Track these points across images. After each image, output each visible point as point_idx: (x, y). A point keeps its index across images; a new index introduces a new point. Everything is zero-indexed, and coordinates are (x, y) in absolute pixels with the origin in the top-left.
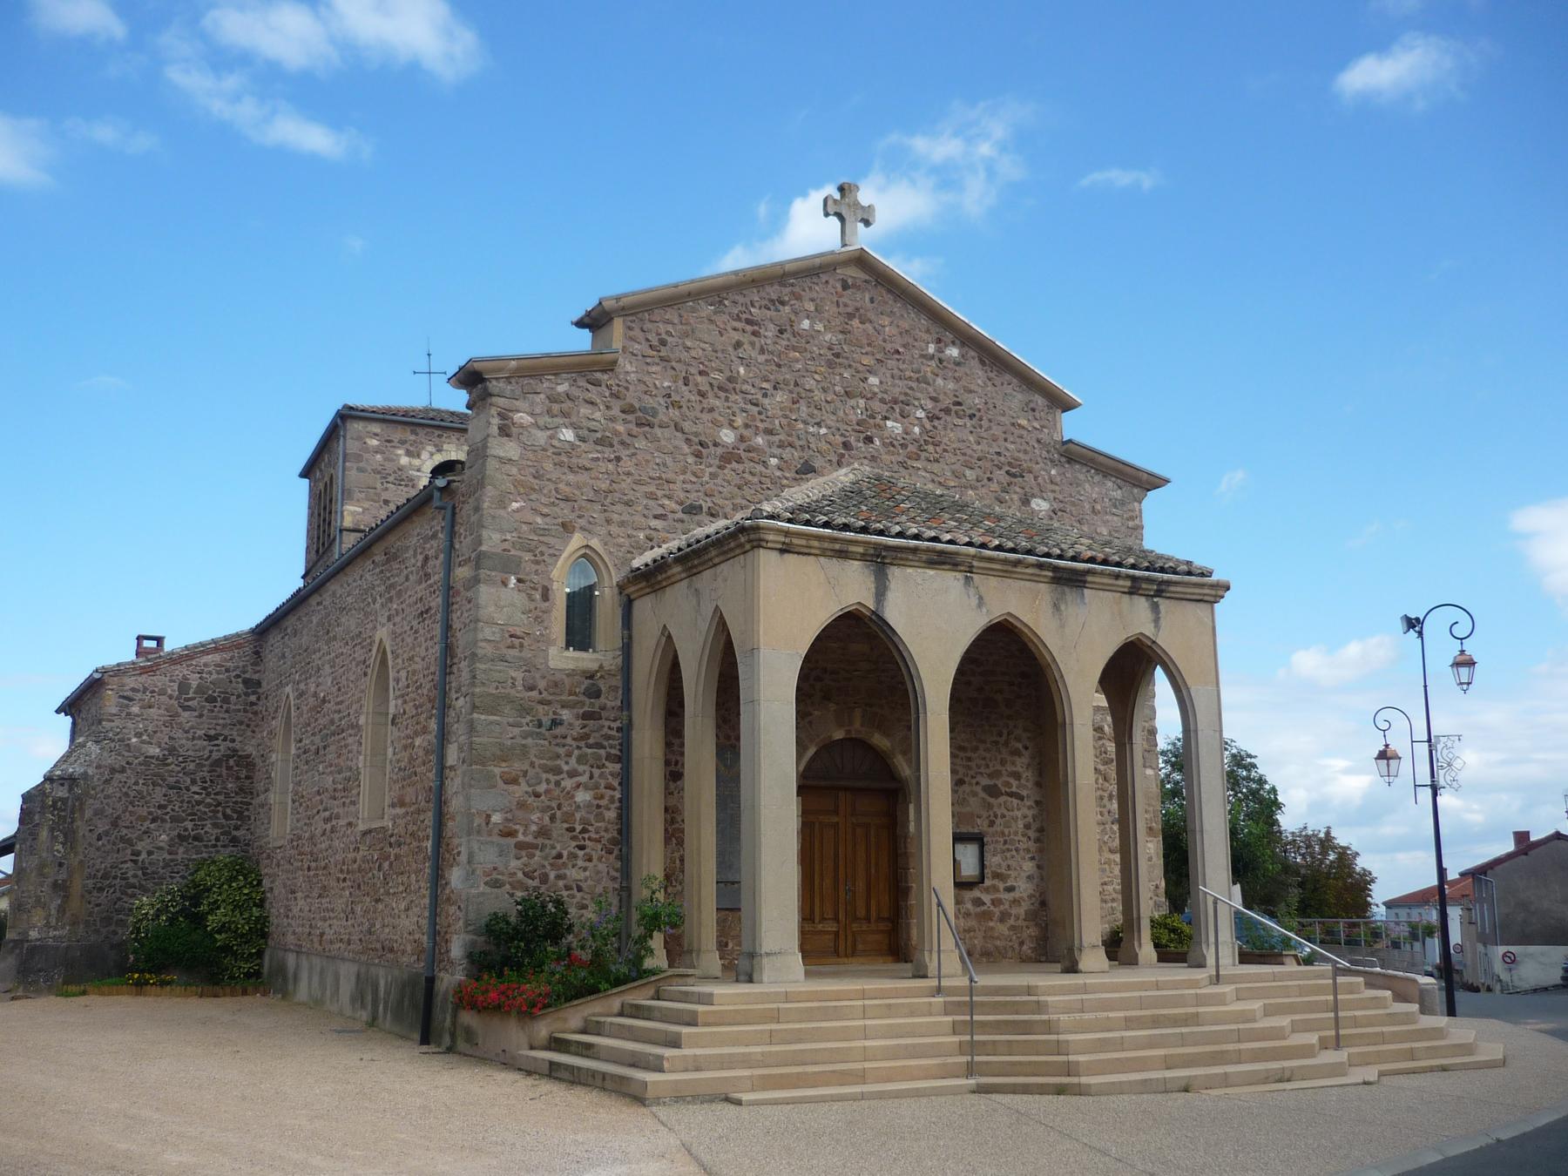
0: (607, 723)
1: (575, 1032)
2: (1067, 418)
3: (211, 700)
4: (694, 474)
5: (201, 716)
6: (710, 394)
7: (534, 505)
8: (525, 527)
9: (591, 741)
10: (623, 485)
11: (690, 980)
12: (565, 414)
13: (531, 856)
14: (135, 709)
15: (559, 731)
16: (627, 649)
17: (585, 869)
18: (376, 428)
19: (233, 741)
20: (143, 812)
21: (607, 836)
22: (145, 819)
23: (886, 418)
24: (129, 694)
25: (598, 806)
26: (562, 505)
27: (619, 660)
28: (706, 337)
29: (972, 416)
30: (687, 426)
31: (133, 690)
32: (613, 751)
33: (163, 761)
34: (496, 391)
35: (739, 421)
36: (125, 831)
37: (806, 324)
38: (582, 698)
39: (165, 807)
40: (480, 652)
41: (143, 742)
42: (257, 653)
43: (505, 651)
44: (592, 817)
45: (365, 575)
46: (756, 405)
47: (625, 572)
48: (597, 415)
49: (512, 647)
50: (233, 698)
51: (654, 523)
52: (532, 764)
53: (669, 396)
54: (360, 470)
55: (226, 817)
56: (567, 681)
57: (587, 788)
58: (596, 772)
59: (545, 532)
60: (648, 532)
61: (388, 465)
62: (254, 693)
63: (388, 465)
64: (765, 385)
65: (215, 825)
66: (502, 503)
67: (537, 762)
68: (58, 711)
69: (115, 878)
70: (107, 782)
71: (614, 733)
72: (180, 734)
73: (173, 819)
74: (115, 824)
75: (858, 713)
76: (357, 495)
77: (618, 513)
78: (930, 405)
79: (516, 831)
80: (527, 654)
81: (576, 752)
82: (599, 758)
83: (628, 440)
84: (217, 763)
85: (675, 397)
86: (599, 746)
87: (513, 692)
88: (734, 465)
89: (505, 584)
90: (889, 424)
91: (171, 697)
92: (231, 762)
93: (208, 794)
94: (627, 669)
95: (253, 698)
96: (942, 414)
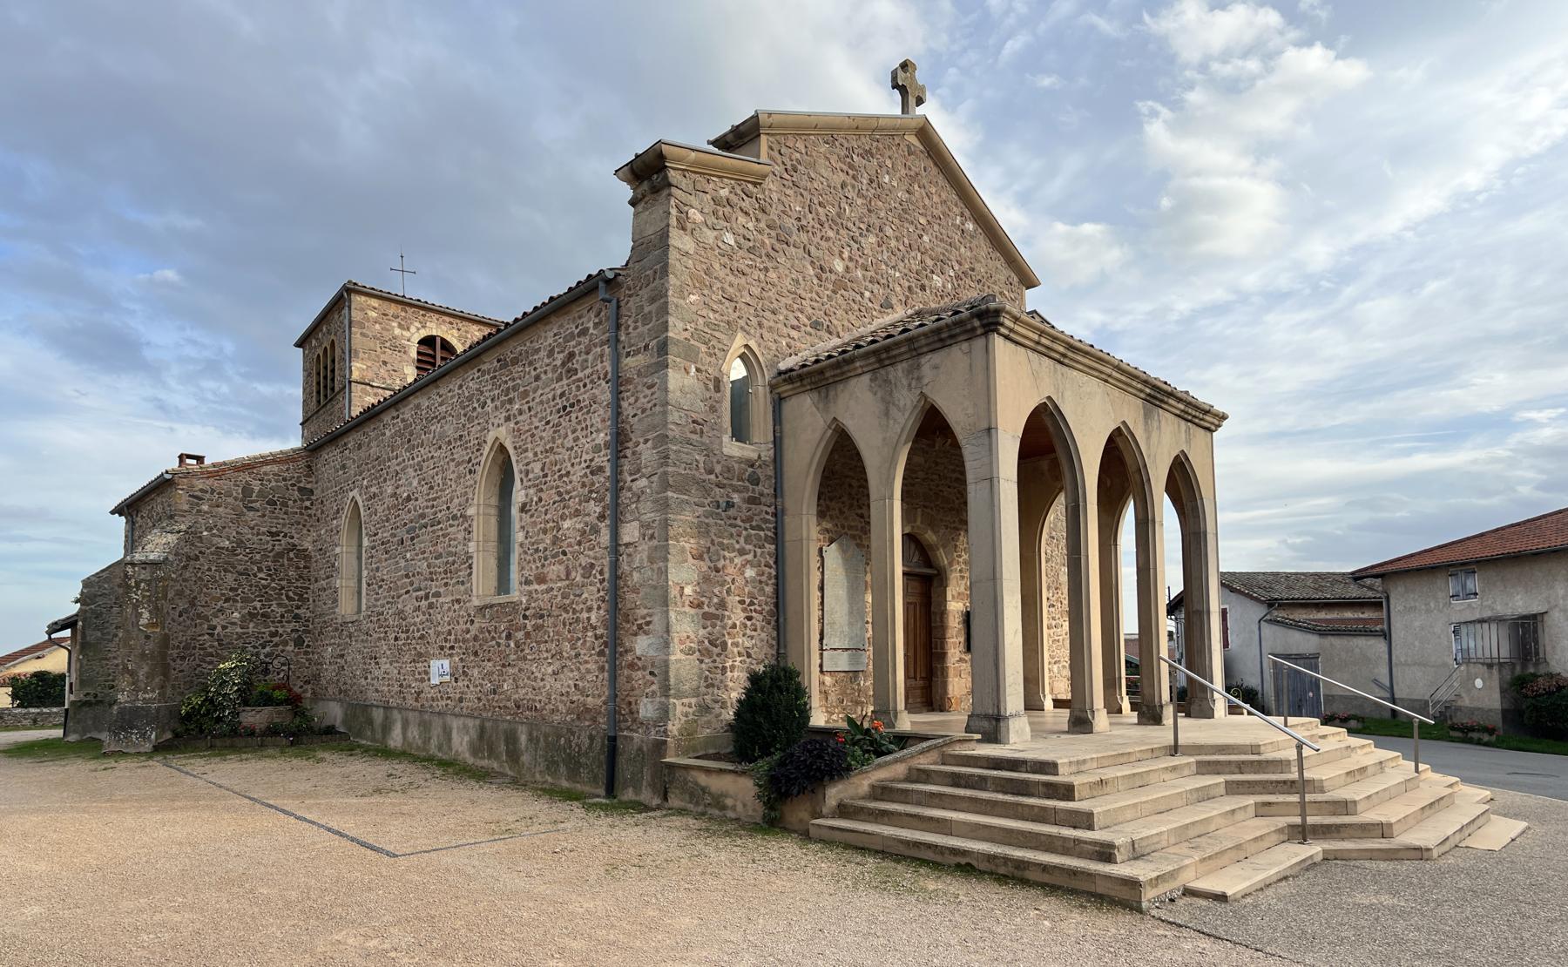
2: (1029, 293)
3: (272, 503)
7: (707, 300)
8: (701, 321)
11: (966, 745)
13: (714, 626)
14: (205, 508)
15: (732, 512)
16: (778, 443)
18: (374, 302)
26: (727, 303)
28: (823, 171)
30: (813, 249)
34: (673, 181)
35: (846, 255)
40: (670, 433)
45: (471, 381)
47: (775, 371)
48: (750, 225)
52: (713, 542)
59: (716, 327)
65: (279, 605)
70: (185, 567)
72: (246, 530)
74: (192, 604)
80: (705, 440)
83: (772, 253)
84: (280, 555)
95: (308, 503)
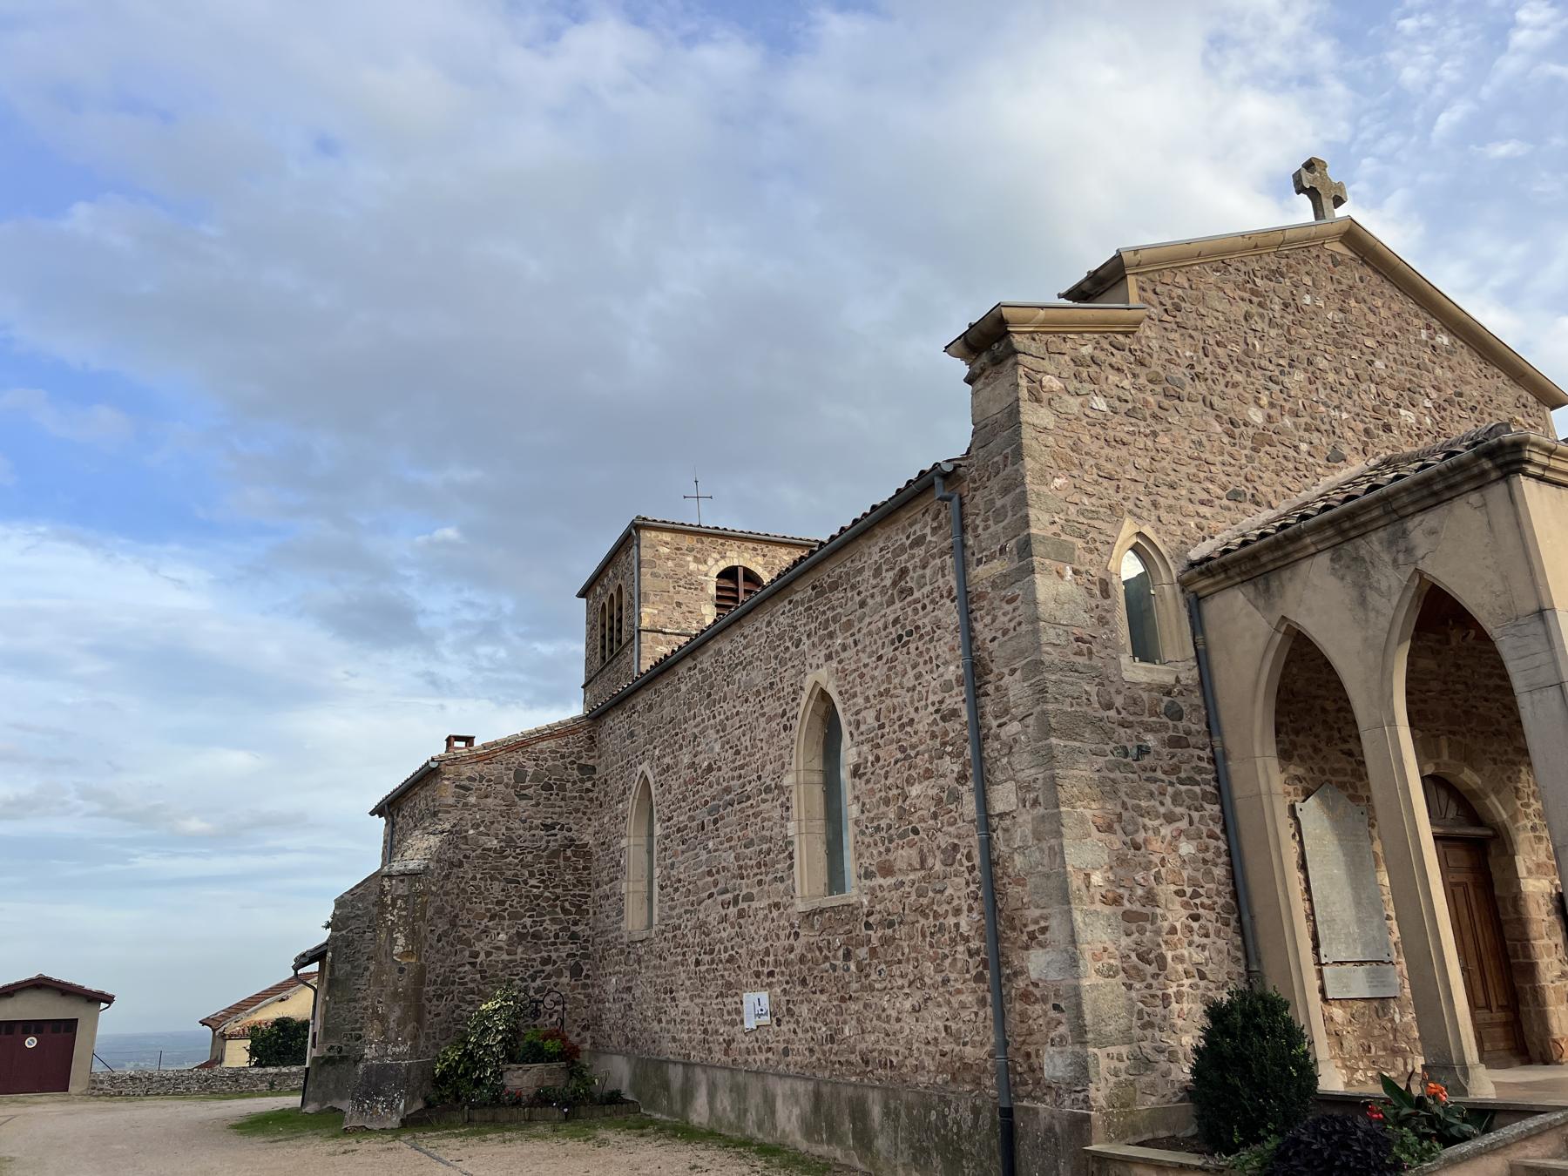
0: (1197, 752)
2: (1557, 416)
4: (1231, 455)
5: (538, 804)
6: (1231, 368)
7: (1078, 482)
8: (1073, 509)
10: (1164, 463)
13: (1142, 931)
14: (472, 800)
15: (1147, 761)
18: (666, 537)
19: (570, 830)
21: (1220, 901)
22: (484, 916)
24: (466, 783)
25: (1205, 861)
26: (1106, 483)
27: (1195, 672)
29: (1473, 409)
30: (1216, 400)
32: (1209, 789)
33: (501, 853)
34: (1020, 347)
35: (1264, 401)
36: (463, 931)
37: (1308, 299)
38: (1165, 719)
39: (503, 903)
40: (1046, 658)
41: (481, 834)
42: (591, 738)
44: (1199, 875)
45: (781, 616)
48: (1126, 383)
49: (1079, 653)
50: (569, 785)
51: (1204, 510)
53: (1192, 367)
56: (1145, 696)
57: (1189, 838)
58: (1195, 815)
60: (1198, 519)
61: (679, 570)
62: (589, 779)
63: (679, 570)
64: (1281, 362)
65: (553, 921)
66: (1043, 479)
68: (372, 813)
69: (453, 983)
71: (1205, 764)
75: (1444, 741)
76: (652, 598)
77: (1166, 497)
81: (1169, 789)
82: (1194, 796)
83: (1160, 413)
84: (555, 854)
85: (1199, 369)
86: (1191, 781)
87: (1090, 711)
88: (1267, 448)
93: (546, 888)
94: (1206, 682)
95: (589, 785)
96: (1446, 405)
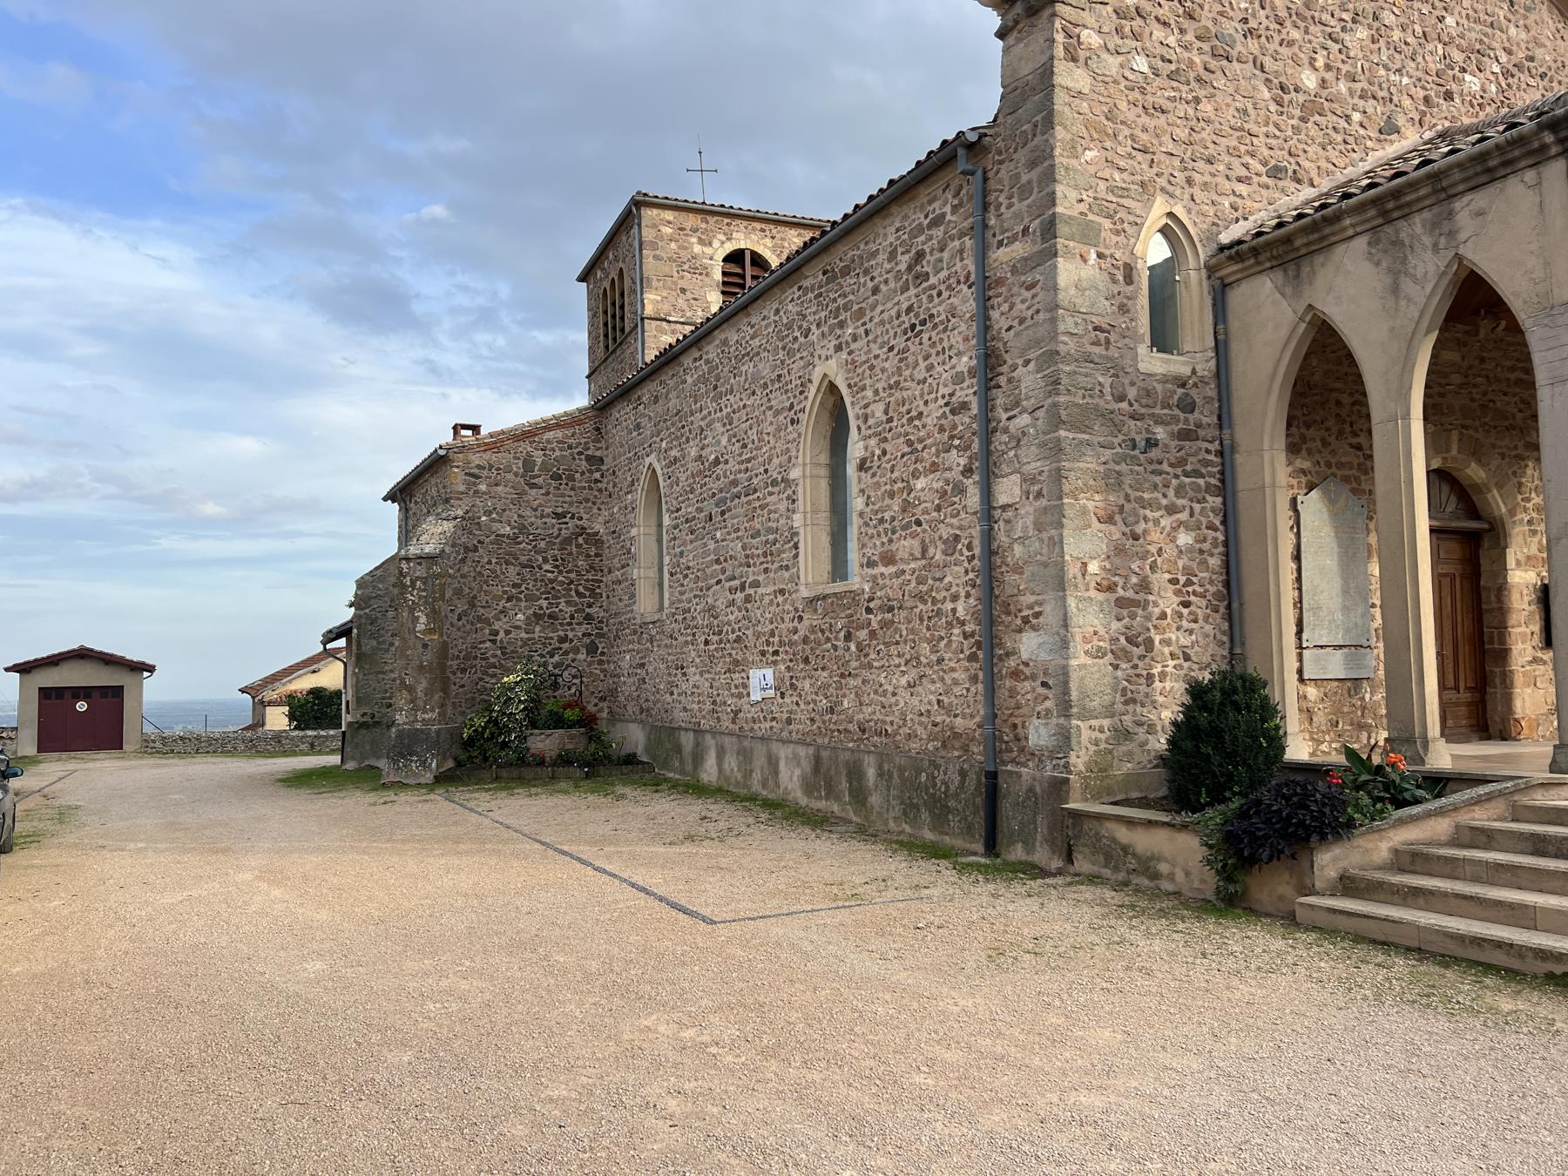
1: (1380, 868)
4: (1277, 126)
5: (548, 493)
6: (1288, 23)
7: (1110, 155)
8: (1102, 186)
9: (1189, 468)
10: (1204, 135)
12: (1136, 37)
13: (1133, 616)
14: (483, 487)
15: (1154, 453)
17: (1191, 632)
18: (669, 215)
20: (498, 591)
21: (1212, 589)
23: (1464, 70)
25: (1201, 552)
27: (1213, 363)
30: (1268, 62)
31: (479, 467)
32: (1213, 481)
33: (514, 539)
35: (1320, 63)
38: (1177, 412)
39: (519, 586)
40: (1062, 349)
41: (493, 520)
42: (598, 429)
43: (1090, 349)
45: (790, 303)
46: (1336, 41)
48: (1172, 40)
49: (1096, 343)
54: (656, 257)
55: (578, 594)
56: (1159, 387)
57: (1188, 528)
58: (1197, 507)
59: (1124, 192)
60: (1233, 199)
61: (683, 253)
63: (683, 253)
67: (1133, 494)
68: (385, 499)
71: (1211, 457)
72: (528, 513)
73: (529, 598)
75: (1455, 435)
76: (655, 283)
78: (1504, 58)
79: (1116, 585)
82: (1197, 488)
83: (1206, 76)
84: (567, 541)
85: (1253, 24)
87: (1102, 403)
88: (1317, 118)
89: (1084, 260)
90: (1468, 77)
91: (516, 475)
92: (580, 540)
93: (560, 572)
95: (597, 475)
